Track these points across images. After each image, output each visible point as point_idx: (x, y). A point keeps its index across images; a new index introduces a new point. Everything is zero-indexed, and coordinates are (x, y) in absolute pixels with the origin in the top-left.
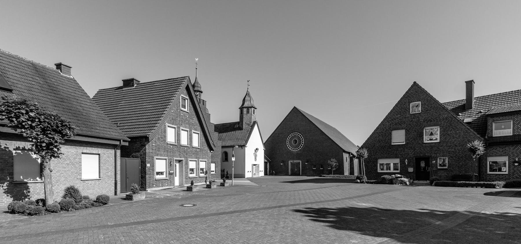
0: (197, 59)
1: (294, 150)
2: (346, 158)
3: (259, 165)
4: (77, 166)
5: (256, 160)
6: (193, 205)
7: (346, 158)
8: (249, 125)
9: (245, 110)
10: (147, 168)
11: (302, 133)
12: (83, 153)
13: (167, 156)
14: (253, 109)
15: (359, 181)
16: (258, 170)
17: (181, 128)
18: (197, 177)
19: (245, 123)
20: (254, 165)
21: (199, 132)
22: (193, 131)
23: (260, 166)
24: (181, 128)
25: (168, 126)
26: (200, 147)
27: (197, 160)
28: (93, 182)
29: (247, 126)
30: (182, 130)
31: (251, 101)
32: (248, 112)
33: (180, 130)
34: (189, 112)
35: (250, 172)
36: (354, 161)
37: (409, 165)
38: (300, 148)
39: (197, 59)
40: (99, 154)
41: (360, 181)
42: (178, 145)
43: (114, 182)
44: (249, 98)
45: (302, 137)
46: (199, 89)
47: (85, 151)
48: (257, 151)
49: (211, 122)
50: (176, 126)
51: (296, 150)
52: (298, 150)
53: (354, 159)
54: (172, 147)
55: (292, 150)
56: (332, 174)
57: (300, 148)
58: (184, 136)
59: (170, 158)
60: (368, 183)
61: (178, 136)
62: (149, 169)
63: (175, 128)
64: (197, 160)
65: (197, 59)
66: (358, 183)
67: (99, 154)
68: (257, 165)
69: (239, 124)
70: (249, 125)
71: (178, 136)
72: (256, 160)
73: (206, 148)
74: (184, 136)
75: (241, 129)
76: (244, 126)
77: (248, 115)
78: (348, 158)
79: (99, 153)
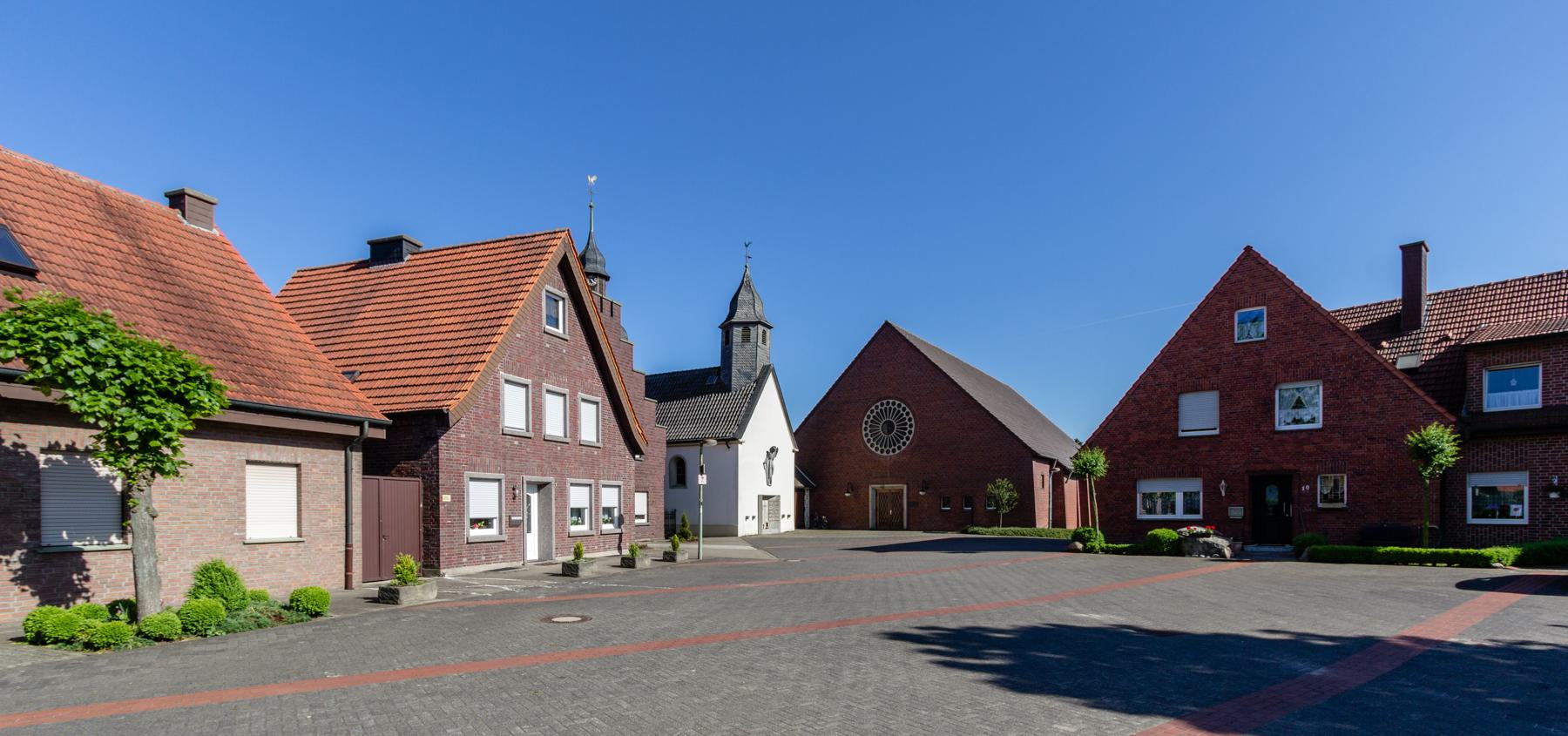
0: (592, 179)
1: (885, 454)
2: (1043, 476)
3: (779, 496)
4: (232, 499)
5: (769, 482)
6: (579, 619)
7: (1043, 476)
8: (748, 376)
9: (737, 331)
10: (442, 508)
11: (910, 402)
12: (249, 462)
13: (504, 471)
14: (761, 328)
15: (1080, 546)
16: (775, 513)
17: (546, 386)
18: (594, 532)
19: (738, 370)
20: (766, 497)
21: (599, 399)
22: (581, 395)
23: (781, 500)
24: (546, 386)
25: (507, 381)
26: (600, 445)
27: (591, 481)
28: (281, 549)
29: (743, 381)
30: (548, 391)
31: (754, 306)
32: (746, 338)
33: (540, 391)
34: (567, 337)
35: (753, 517)
36: (1065, 485)
37: (1231, 500)
38: (903, 448)
39: (591, 177)
40: (297, 466)
41: (1085, 545)
42: (534, 434)
43: (343, 548)
44: (751, 296)
45: (908, 414)
46: (599, 269)
47: (255, 456)
48: (772, 455)
49: (635, 369)
50: (529, 381)
51: (891, 454)
52: (897, 451)
53: (1065, 479)
54: (516, 443)
55: (879, 452)
56: (999, 526)
57: (903, 448)
58: (554, 409)
59: (511, 476)
60: (1106, 551)
61: (536, 412)
62: (449, 511)
63: (526, 386)
64: (591, 481)
65: (592, 179)
66: (1077, 551)
67: (297, 466)
68: (774, 498)
69: (719, 374)
70: (748, 376)
71: (536, 412)
72: (769, 482)
73: (621, 446)
74: (554, 409)
75: (724, 387)
76: (736, 380)
77: (748, 346)
78: (1046, 478)
79: (299, 461)
